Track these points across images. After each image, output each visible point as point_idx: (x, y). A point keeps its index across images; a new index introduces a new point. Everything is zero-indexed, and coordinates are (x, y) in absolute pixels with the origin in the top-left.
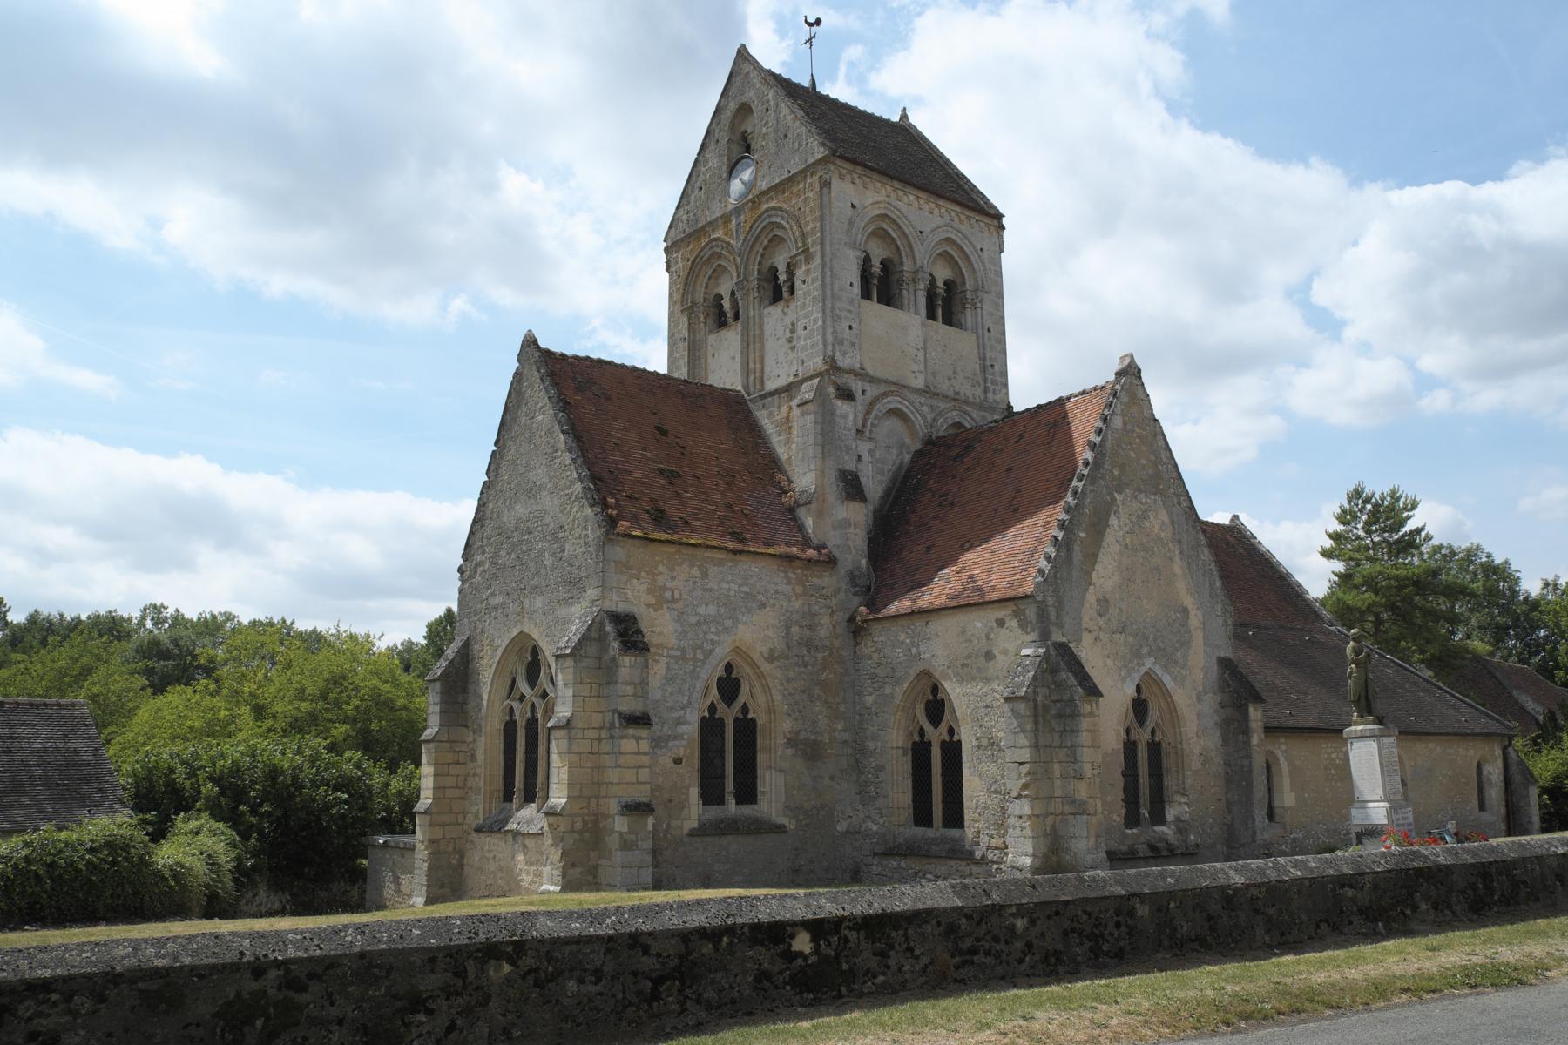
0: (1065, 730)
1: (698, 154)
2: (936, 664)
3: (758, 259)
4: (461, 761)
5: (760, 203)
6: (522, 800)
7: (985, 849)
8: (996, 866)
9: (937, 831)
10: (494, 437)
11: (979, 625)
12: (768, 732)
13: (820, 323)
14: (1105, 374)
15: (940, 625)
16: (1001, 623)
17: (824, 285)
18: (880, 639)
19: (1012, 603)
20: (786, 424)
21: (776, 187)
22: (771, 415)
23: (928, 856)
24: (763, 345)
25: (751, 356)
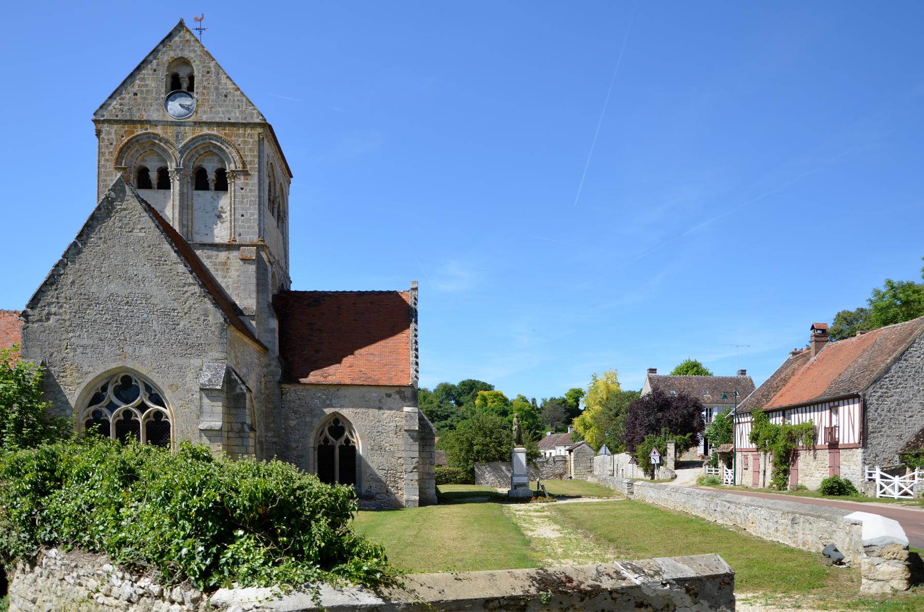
0: (426, 445)
11: (374, 395)
13: (256, 216)
16: (389, 396)
17: (260, 197)
18: (302, 394)
24: (192, 212)
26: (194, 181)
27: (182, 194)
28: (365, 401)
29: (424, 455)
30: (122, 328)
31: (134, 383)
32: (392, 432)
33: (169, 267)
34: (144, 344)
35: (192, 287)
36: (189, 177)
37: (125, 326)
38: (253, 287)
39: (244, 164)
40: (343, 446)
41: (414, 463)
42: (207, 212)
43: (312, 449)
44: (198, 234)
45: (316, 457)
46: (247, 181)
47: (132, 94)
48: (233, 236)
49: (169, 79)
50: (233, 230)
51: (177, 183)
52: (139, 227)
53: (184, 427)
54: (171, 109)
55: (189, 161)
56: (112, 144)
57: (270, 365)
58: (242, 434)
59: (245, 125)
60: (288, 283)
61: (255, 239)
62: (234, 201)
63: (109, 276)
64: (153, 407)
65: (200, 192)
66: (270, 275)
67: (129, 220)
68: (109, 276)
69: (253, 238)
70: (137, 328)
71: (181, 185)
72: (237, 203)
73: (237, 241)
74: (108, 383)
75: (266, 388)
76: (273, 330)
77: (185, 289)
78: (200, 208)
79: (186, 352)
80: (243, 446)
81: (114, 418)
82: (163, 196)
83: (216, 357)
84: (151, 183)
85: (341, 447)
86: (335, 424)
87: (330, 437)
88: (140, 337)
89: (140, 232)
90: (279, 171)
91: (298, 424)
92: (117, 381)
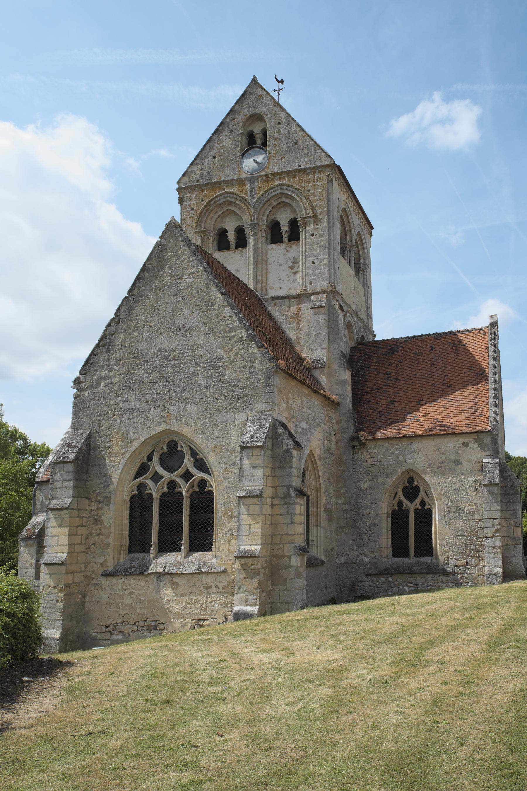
0: (509, 502)
1: (213, 135)
2: (418, 466)
3: (268, 213)
4: (84, 524)
5: (273, 179)
6: (157, 551)
7: (453, 567)
8: (461, 575)
9: (412, 559)
12: (315, 503)
13: (326, 262)
15: (418, 445)
16: (466, 445)
17: (329, 240)
18: (374, 451)
19: (476, 435)
20: (297, 318)
21: (288, 173)
22: (281, 311)
23: (412, 573)
25: (259, 273)
27: (256, 250)
29: (508, 514)
30: (167, 386)
31: (179, 448)
32: (471, 489)
33: (216, 312)
34: (189, 402)
35: (238, 332)
36: (263, 231)
37: (171, 384)
38: (323, 337)
39: (313, 208)
40: (418, 509)
41: (495, 525)
42: (280, 265)
43: (386, 515)
44: (273, 288)
45: (390, 525)
47: (211, 157)
48: (304, 285)
49: (244, 138)
50: (304, 279)
51: (252, 238)
52: (188, 272)
53: (227, 496)
54: (246, 166)
55: (263, 216)
56: (192, 209)
57: (341, 421)
58: (287, 500)
59: (313, 169)
61: (325, 285)
62: (305, 249)
63: (158, 330)
64: (199, 475)
65: (274, 246)
66: (341, 323)
67: (179, 267)
68: (158, 330)
69: (324, 285)
70: (182, 384)
71: (256, 241)
73: (308, 290)
74: (153, 452)
75: (337, 448)
76: (343, 383)
78: (274, 262)
79: (231, 406)
82: (240, 255)
83: (262, 409)
84: (229, 243)
85: (416, 511)
86: (409, 484)
87: (404, 500)
88: (186, 394)
89: (189, 277)
90: (356, 220)
91: (370, 487)
92: (163, 448)
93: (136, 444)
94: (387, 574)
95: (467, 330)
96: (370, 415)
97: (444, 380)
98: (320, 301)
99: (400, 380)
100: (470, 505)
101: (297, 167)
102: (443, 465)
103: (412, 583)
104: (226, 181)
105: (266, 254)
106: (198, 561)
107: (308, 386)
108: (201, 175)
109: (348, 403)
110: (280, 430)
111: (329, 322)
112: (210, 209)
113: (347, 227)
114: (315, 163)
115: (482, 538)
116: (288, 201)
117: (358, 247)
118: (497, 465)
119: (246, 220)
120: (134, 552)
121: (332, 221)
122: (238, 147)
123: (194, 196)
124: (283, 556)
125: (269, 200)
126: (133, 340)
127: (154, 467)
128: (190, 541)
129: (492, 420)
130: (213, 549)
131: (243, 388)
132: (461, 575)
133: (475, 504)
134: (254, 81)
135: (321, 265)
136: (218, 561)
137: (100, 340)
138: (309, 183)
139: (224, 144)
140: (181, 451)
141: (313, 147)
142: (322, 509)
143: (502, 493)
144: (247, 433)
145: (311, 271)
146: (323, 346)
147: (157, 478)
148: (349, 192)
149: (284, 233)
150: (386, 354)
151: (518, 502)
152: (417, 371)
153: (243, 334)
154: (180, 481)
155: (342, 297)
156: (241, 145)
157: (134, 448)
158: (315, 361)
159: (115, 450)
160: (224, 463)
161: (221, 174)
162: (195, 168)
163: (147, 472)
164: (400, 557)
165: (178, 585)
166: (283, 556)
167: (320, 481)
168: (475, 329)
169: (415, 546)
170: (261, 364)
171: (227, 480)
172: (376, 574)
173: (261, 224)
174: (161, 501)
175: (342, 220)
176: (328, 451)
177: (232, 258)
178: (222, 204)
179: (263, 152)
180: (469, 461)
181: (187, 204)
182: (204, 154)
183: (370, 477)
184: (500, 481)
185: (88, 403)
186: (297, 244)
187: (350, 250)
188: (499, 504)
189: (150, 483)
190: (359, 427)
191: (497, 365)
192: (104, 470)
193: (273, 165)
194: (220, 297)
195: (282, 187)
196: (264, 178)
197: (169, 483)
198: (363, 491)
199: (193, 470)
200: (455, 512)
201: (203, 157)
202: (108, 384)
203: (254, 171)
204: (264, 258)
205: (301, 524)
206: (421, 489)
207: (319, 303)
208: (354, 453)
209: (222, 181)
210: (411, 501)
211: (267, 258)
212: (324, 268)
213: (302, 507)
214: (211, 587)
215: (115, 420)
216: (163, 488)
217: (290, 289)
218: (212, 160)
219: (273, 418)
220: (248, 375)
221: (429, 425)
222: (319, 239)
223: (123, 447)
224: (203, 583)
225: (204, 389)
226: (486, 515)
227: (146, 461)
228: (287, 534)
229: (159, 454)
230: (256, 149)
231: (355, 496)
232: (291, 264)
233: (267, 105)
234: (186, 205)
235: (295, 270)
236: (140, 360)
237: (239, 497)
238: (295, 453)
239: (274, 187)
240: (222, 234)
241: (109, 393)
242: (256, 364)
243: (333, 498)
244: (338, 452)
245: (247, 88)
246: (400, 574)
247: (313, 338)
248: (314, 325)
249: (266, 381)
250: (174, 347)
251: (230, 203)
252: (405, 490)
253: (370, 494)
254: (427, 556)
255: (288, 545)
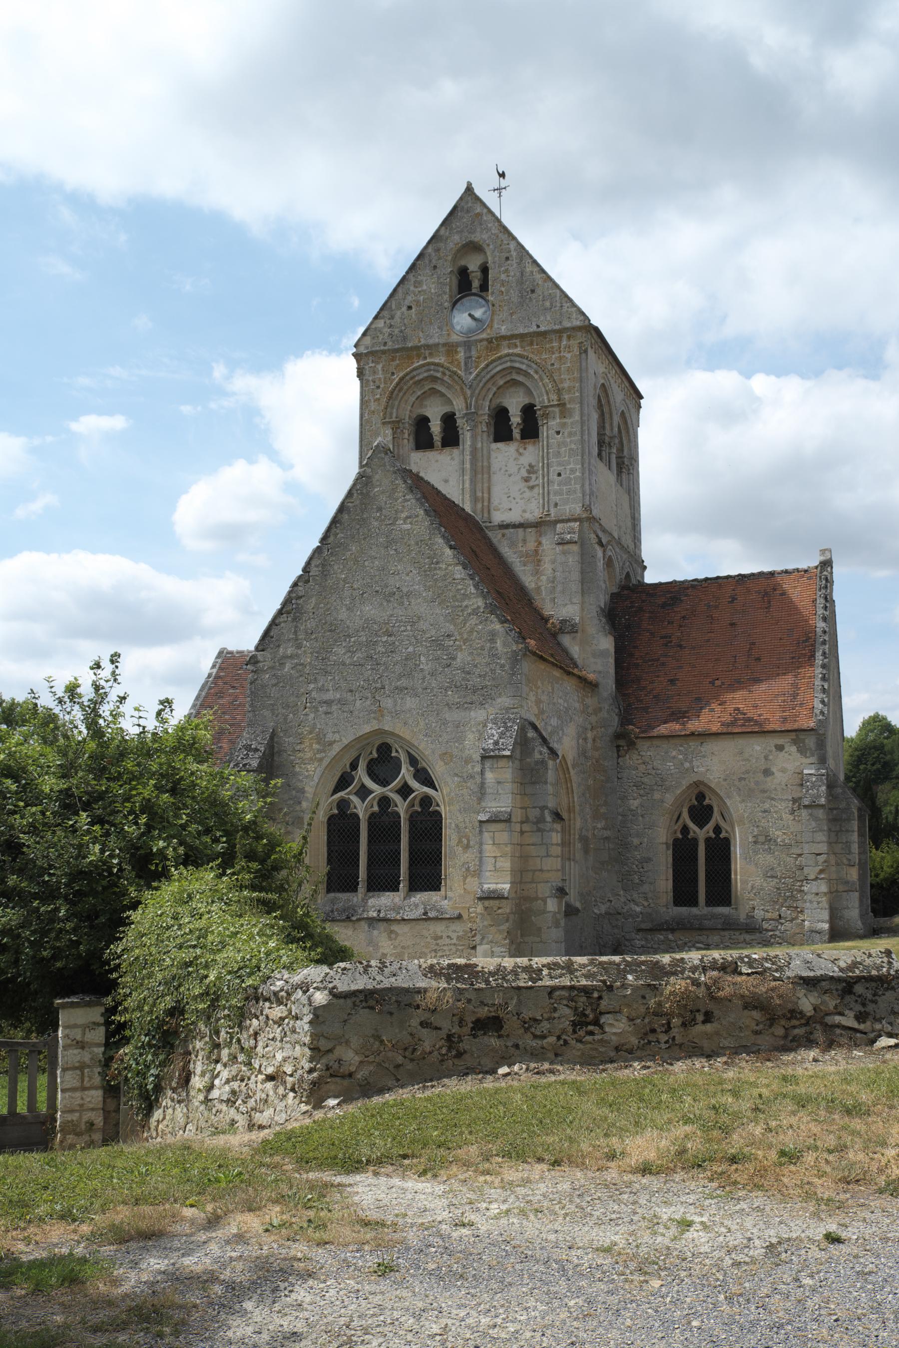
0: (841, 831)
1: (407, 273)
2: (711, 777)
3: (490, 396)
8: (771, 933)
9: (701, 910)
10: (710, 576)
11: (758, 748)
14: (811, 561)
15: (711, 746)
16: (780, 748)
17: (582, 441)
18: (649, 753)
19: (794, 734)
20: (535, 557)
21: (522, 336)
22: (513, 545)
23: (701, 929)
24: (490, 477)
25: (479, 486)
26: (492, 429)
27: (474, 451)
28: (743, 760)
31: (394, 754)
33: (443, 573)
36: (484, 424)
38: (575, 587)
39: (559, 392)
40: (710, 838)
41: (820, 863)
43: (664, 846)
44: (499, 510)
45: (670, 860)
46: (565, 420)
48: (546, 509)
49: (454, 278)
50: (546, 499)
51: (468, 435)
52: (403, 515)
56: (378, 387)
57: (600, 709)
58: (541, 826)
60: (639, 571)
62: (548, 453)
64: (420, 789)
66: (600, 564)
68: (362, 594)
70: (398, 669)
71: (474, 438)
72: (551, 455)
75: (596, 749)
76: (603, 654)
77: (465, 604)
78: (501, 469)
79: (464, 701)
80: (542, 844)
81: (366, 810)
82: (449, 458)
85: (708, 840)
87: (691, 825)
88: (403, 682)
89: (405, 523)
90: (618, 395)
92: (371, 753)
93: (337, 748)
94: (666, 930)
95: (786, 572)
96: (641, 701)
97: (750, 649)
98: (569, 533)
99: (685, 648)
100: (784, 833)
101: (534, 328)
102: (746, 776)
103: (701, 942)
104: (428, 347)
105: (489, 458)
106: (422, 903)
107: (561, 668)
108: (390, 334)
109: (609, 684)
110: (531, 734)
111: (582, 563)
112: (405, 387)
113: (606, 409)
114: (561, 322)
115: (802, 881)
116: (520, 378)
117: (621, 438)
118: (824, 777)
119: (458, 406)
120: (334, 891)
121: (586, 412)
122: (445, 293)
123: (380, 367)
124: (537, 899)
125: (492, 377)
126: (329, 606)
127: (360, 779)
128: (410, 877)
129: (818, 712)
130: (443, 889)
131: (480, 676)
132: (771, 933)
133: (792, 833)
134: (469, 189)
135: (571, 479)
136: (450, 903)
137: (285, 603)
138: (553, 353)
139: (425, 287)
140: (396, 757)
141: (558, 298)
142: (577, 837)
143: (831, 817)
144: (489, 738)
145: (556, 487)
146: (575, 600)
147: (363, 792)
148: (610, 357)
149: (515, 425)
150: (664, 606)
151: (853, 831)
152: (710, 635)
153: (480, 604)
154: (396, 798)
155: (600, 525)
156: (450, 290)
157: (335, 753)
158: (563, 622)
159: (309, 755)
160: (456, 775)
161: (421, 334)
162: (380, 324)
163: (349, 785)
164: (685, 906)
165: (397, 934)
166: (537, 899)
167: (573, 797)
168: (798, 570)
169: (706, 891)
170: (505, 644)
171: (461, 798)
172: (651, 930)
173: (480, 412)
174: (369, 823)
175: (600, 405)
176: (583, 753)
177: (437, 461)
178: (422, 380)
179: (483, 302)
180: (783, 770)
181: (370, 378)
182: (394, 302)
183: (642, 792)
184: (829, 801)
185: (268, 690)
186: (534, 443)
187: (609, 444)
188: (825, 833)
189: (355, 799)
190: (626, 719)
191: (827, 629)
192: (294, 781)
193: (498, 324)
194: (448, 552)
195: (513, 358)
196: (485, 343)
197: (380, 800)
198: (632, 810)
199: (414, 784)
200: (763, 843)
201: (394, 307)
202: (297, 664)
203: (470, 331)
204: (485, 464)
205: (557, 857)
206: (716, 809)
207: (568, 537)
208: (619, 756)
209: (422, 346)
210: (701, 827)
211: (489, 463)
212: (575, 484)
213: (559, 834)
214: (441, 937)
215: (306, 715)
216: (372, 807)
217: (524, 511)
218: (406, 312)
219: (521, 718)
220: (487, 660)
221: (727, 718)
222: (568, 440)
223: (319, 751)
224: (431, 932)
225: (428, 677)
226: (807, 848)
227: (349, 771)
228: (541, 870)
229: (367, 761)
230: (473, 297)
231: (620, 817)
232: (526, 475)
233: (488, 230)
234: (368, 381)
235: (531, 483)
236: (339, 633)
237: (481, 822)
238: (551, 763)
239: (500, 358)
240: (422, 422)
241: (298, 678)
242: (499, 644)
243: (589, 820)
244: (596, 754)
245: (458, 202)
246: (685, 929)
247: (559, 588)
248: (561, 569)
249: (512, 669)
250: (386, 618)
251: (434, 379)
252: (692, 810)
253: (642, 816)
254: (723, 906)
255: (542, 884)
